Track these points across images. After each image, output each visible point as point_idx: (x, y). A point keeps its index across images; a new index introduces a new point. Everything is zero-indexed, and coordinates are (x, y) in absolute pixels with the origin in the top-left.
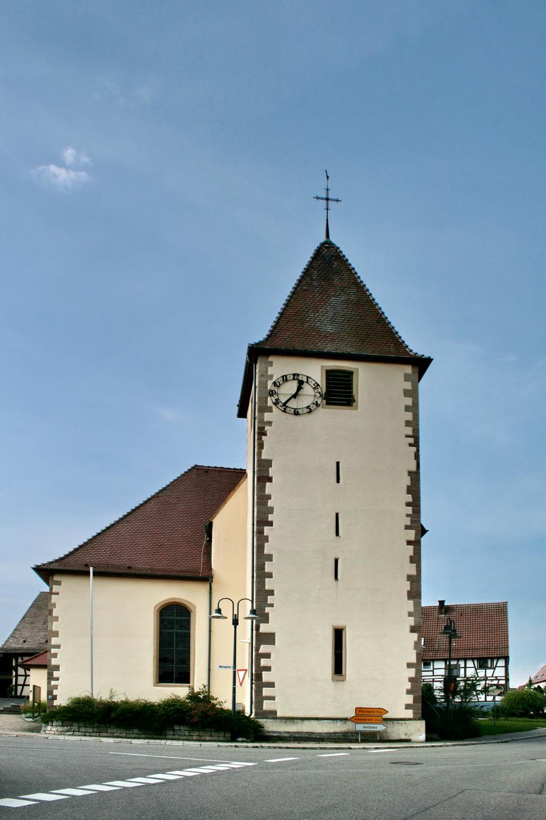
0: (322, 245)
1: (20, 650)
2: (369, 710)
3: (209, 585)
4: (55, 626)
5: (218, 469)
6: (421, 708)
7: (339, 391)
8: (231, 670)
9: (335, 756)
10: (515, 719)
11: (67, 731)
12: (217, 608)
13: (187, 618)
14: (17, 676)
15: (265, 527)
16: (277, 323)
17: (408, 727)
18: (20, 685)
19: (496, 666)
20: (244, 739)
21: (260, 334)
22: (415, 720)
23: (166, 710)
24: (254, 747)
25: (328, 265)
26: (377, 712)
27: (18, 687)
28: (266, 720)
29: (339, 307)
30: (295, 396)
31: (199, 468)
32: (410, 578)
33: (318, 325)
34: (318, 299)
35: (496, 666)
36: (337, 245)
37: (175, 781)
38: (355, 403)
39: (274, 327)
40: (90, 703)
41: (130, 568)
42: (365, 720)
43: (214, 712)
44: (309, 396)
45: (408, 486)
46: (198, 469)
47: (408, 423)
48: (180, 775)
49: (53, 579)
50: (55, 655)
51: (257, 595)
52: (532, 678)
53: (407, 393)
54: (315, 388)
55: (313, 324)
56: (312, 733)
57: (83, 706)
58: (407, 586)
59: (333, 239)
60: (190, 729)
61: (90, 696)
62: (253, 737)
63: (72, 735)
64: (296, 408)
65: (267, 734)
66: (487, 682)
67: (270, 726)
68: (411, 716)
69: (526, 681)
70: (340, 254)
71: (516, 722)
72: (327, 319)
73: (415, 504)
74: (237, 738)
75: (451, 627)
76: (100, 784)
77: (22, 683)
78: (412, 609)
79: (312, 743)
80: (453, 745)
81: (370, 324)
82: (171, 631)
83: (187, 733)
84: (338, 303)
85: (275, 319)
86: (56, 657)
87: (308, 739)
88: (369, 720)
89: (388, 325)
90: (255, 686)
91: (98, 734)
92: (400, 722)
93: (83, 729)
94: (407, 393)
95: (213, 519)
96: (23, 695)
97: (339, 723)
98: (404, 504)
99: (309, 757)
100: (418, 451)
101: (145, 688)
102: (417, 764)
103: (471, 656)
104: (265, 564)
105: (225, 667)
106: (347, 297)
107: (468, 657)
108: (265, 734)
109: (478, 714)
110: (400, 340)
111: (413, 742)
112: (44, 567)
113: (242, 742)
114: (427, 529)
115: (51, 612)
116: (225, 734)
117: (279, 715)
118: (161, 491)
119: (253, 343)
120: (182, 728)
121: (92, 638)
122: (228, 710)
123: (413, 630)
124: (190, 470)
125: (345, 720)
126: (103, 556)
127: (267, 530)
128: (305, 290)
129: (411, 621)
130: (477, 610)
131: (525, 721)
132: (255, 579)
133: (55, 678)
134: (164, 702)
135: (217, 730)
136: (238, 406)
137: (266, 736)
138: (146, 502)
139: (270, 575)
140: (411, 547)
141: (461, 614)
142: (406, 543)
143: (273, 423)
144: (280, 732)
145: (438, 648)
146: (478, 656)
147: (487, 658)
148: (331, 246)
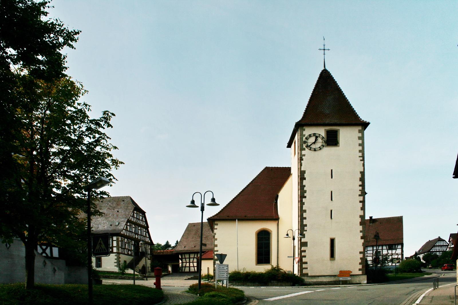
0: (323, 71)
2: (345, 272)
4: (216, 243)
6: (365, 270)
8: (293, 258)
10: (406, 273)
14: (182, 263)
18: (184, 267)
25: (326, 83)
30: (314, 143)
35: (397, 248)
36: (329, 71)
42: (343, 276)
49: (215, 223)
59: (327, 68)
66: (393, 256)
67: (307, 280)
69: (413, 254)
73: (363, 186)
77: (185, 266)
80: (378, 285)
93: (237, 284)
95: (279, 193)
99: (328, 289)
100: (364, 162)
111: (362, 284)
113: (297, 286)
119: (297, 122)
120: (274, 282)
123: (362, 238)
125: (335, 276)
127: (304, 200)
129: (361, 234)
136: (288, 143)
139: (305, 218)
140: (361, 203)
141: (380, 223)
142: (359, 202)
143: (306, 155)
144: (309, 282)
145: (369, 239)
146: (388, 244)
147: (393, 245)
148: (326, 71)
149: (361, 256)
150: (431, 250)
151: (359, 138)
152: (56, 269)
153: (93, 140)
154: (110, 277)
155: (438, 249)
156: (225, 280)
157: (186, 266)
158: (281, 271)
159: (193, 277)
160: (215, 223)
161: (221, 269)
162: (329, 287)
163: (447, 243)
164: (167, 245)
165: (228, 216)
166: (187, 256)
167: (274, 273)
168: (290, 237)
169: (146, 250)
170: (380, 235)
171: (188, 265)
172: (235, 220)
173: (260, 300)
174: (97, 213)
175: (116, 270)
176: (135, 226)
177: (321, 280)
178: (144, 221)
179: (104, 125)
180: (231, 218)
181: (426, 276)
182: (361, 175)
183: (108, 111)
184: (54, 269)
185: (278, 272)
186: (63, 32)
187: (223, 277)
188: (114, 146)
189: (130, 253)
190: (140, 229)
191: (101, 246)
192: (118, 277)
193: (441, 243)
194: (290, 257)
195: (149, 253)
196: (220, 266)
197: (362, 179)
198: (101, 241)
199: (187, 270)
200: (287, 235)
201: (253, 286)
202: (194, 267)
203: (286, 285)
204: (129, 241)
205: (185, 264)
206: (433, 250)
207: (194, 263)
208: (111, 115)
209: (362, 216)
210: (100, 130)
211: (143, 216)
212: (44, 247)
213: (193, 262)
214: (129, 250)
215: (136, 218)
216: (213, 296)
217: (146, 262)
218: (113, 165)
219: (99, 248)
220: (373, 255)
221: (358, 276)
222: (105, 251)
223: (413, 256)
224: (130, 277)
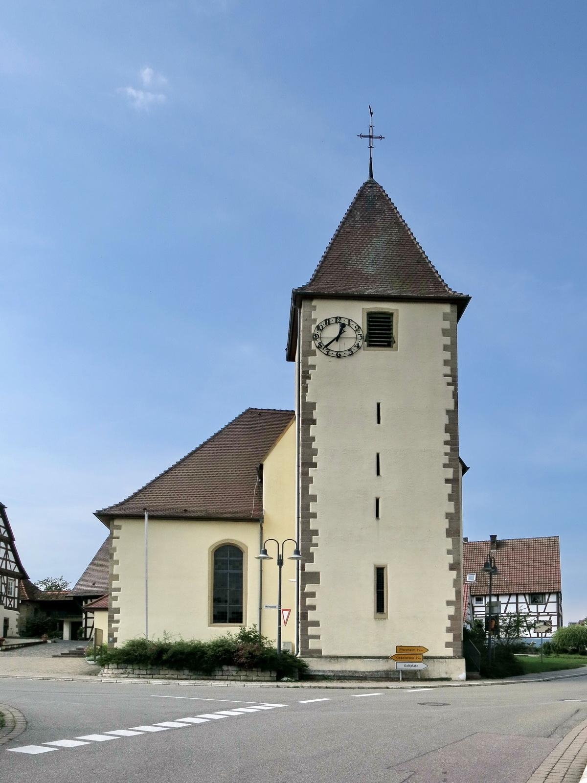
0: (366, 184)
1: (90, 592)
2: (410, 648)
3: (260, 526)
4: (116, 570)
5: (270, 411)
7: (380, 332)
8: (277, 610)
9: (369, 696)
10: (566, 655)
11: (122, 674)
13: (240, 559)
16: (321, 266)
17: (448, 665)
18: (89, 627)
19: (548, 602)
20: (289, 679)
21: (303, 278)
22: (455, 658)
23: (215, 651)
24: (294, 687)
25: (371, 203)
26: (418, 650)
28: (311, 659)
29: (380, 249)
30: (337, 339)
31: (253, 411)
32: (448, 516)
33: (360, 267)
34: (360, 241)
35: (548, 602)
37: (201, 724)
38: (394, 344)
39: (318, 271)
40: (144, 645)
41: (185, 510)
42: (406, 658)
43: (261, 652)
44: (351, 338)
45: (446, 425)
46: (252, 412)
47: (446, 363)
48: (235, 711)
50: (116, 599)
51: (302, 536)
53: (445, 332)
54: (356, 330)
55: (355, 267)
56: (355, 672)
57: (137, 648)
58: (445, 524)
61: (145, 637)
62: (298, 676)
63: (127, 677)
64: (338, 351)
65: (313, 673)
67: (315, 665)
68: (452, 654)
70: (383, 193)
71: (565, 660)
72: (369, 262)
73: (453, 443)
74: (283, 677)
75: (491, 565)
76: (127, 729)
78: (451, 547)
79: (354, 681)
80: (492, 684)
81: (410, 264)
82: (225, 571)
84: (380, 244)
85: (318, 263)
87: (351, 678)
88: (409, 658)
89: (428, 265)
90: (301, 625)
91: (151, 676)
92: (441, 660)
93: (137, 672)
94: (445, 332)
95: (264, 461)
97: (381, 662)
98: (442, 443)
100: (456, 389)
101: (202, 630)
102: (444, 704)
103: (522, 592)
104: (309, 505)
105: (271, 607)
106: (388, 238)
108: (311, 673)
109: (530, 651)
110: (439, 279)
112: (105, 512)
113: (287, 681)
114: (468, 467)
115: (111, 556)
116: (271, 673)
117: (323, 654)
118: (217, 435)
120: (230, 668)
121: (147, 581)
122: (275, 650)
124: (244, 413)
126: (159, 501)
127: (311, 471)
128: (349, 232)
129: (450, 559)
130: (528, 545)
131: (576, 658)
132: (300, 519)
133: (115, 621)
134: (213, 643)
135: (263, 670)
137: (312, 675)
138: (202, 446)
139: (314, 516)
141: (513, 549)
143: (316, 366)
144: (324, 671)
146: (530, 592)
148: (374, 185)
177: (353, 669)
195: (16, 596)
203: (260, 678)
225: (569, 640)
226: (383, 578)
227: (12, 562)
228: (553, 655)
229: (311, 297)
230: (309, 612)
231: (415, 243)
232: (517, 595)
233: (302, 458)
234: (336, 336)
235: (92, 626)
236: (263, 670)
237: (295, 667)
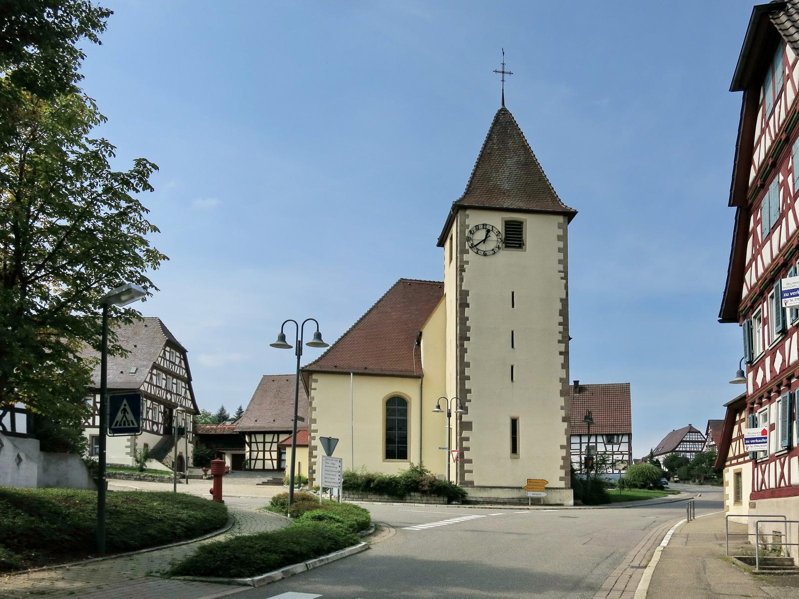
0: (500, 111)
2: (536, 481)
6: (570, 480)
10: (637, 490)
12: (437, 405)
13: (405, 408)
14: (251, 451)
15: (465, 342)
19: (621, 442)
20: (457, 503)
25: (504, 128)
27: (252, 461)
30: (484, 241)
35: (621, 442)
42: (534, 488)
52: (653, 450)
60: (421, 495)
67: (472, 494)
68: (563, 486)
69: (648, 453)
71: (638, 493)
73: (565, 324)
74: (453, 501)
80: (593, 509)
82: (394, 418)
83: (419, 498)
86: (315, 440)
92: (556, 490)
93: (352, 496)
96: (256, 468)
97: (516, 491)
98: (558, 324)
107: (598, 433)
111: (566, 506)
113: (455, 504)
117: (475, 485)
120: (416, 494)
122: (585, 481)
123: (564, 420)
129: (563, 413)
138: (370, 312)
139: (468, 378)
140: (562, 357)
142: (559, 354)
146: (606, 433)
149: (563, 453)
150: (677, 449)
151: (560, 238)
152: (23, 456)
153: (114, 211)
154: (117, 476)
155: (688, 446)
156: (337, 487)
157: (258, 458)
158: (427, 474)
159: (271, 479)
160: (313, 378)
161: (330, 467)
162: (510, 509)
163: (704, 438)
164: (222, 417)
165: (336, 367)
166: (260, 438)
167: (416, 477)
168: (443, 412)
169: (186, 423)
170: (594, 416)
171: (261, 455)
172: (349, 374)
173: (397, 529)
174: (118, 350)
175: (129, 461)
176: (166, 377)
178: (183, 368)
179: (137, 185)
180: (341, 370)
181: (671, 497)
182: (562, 304)
183: (146, 160)
184: (18, 456)
185: (422, 476)
186: (81, 10)
187: (333, 481)
188: (152, 225)
189: (155, 428)
190: (175, 382)
191: (126, 414)
192: (132, 475)
193: (694, 437)
194: (443, 449)
195: (191, 431)
196: (328, 461)
197: (564, 312)
198: (125, 405)
199: (259, 465)
200: (438, 407)
201: (380, 502)
202: (272, 460)
203: (436, 502)
204: (154, 406)
205: (256, 453)
206: (681, 449)
207: (272, 452)
208: (151, 167)
209: (564, 379)
210: (131, 194)
211: (182, 357)
212: (86, 424)
213: (270, 451)
214: (154, 423)
215: (170, 361)
216: (320, 518)
217: (185, 447)
218: (148, 262)
219: (122, 419)
220: (581, 452)
221: (558, 490)
222: (133, 424)
223: (646, 458)
224: (156, 477)
225: (639, 476)
226: (516, 427)
227: (189, 400)
228: (626, 489)
229: (465, 208)
230: (465, 452)
231: (537, 164)
232: (596, 435)
233: (460, 333)
234: (484, 239)
235: (255, 458)
236: (439, 496)
237: (459, 493)
